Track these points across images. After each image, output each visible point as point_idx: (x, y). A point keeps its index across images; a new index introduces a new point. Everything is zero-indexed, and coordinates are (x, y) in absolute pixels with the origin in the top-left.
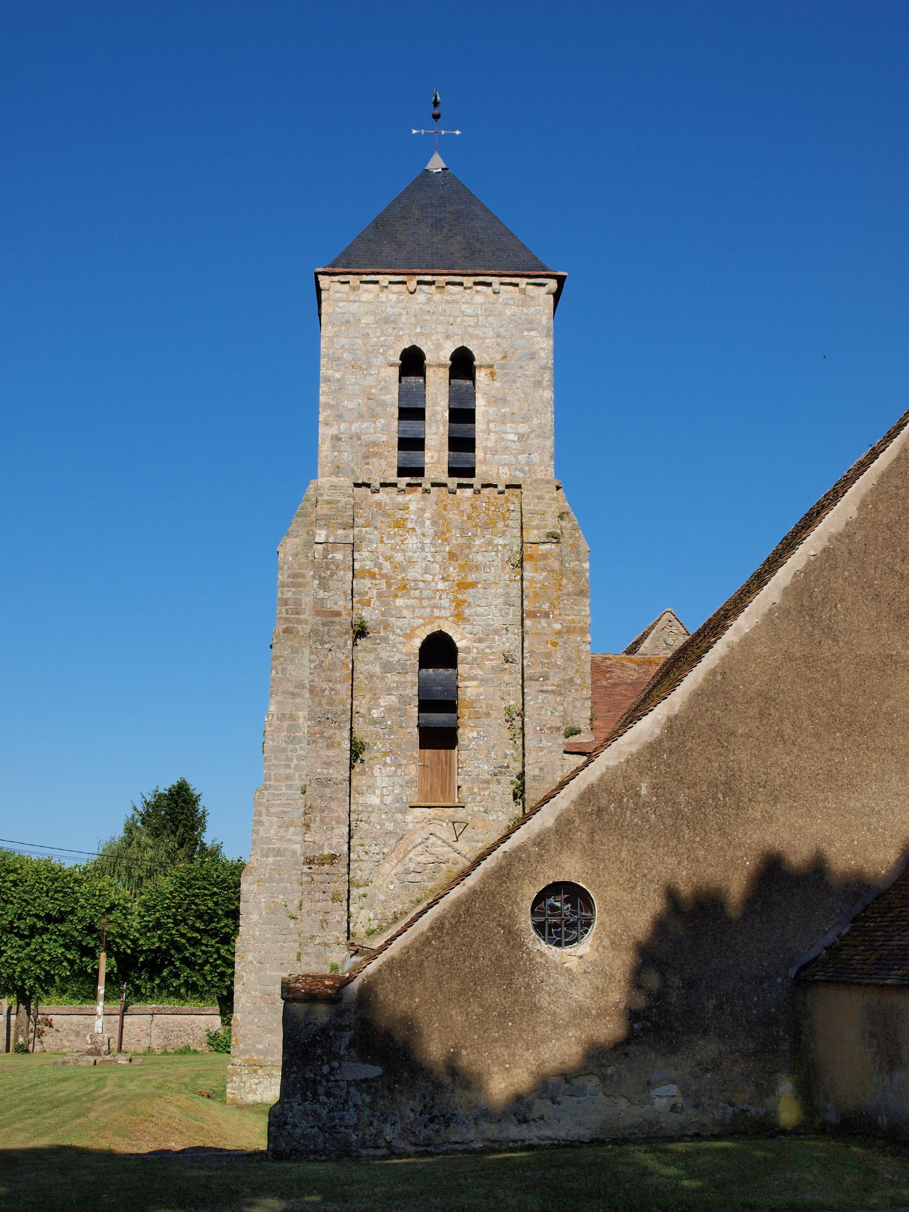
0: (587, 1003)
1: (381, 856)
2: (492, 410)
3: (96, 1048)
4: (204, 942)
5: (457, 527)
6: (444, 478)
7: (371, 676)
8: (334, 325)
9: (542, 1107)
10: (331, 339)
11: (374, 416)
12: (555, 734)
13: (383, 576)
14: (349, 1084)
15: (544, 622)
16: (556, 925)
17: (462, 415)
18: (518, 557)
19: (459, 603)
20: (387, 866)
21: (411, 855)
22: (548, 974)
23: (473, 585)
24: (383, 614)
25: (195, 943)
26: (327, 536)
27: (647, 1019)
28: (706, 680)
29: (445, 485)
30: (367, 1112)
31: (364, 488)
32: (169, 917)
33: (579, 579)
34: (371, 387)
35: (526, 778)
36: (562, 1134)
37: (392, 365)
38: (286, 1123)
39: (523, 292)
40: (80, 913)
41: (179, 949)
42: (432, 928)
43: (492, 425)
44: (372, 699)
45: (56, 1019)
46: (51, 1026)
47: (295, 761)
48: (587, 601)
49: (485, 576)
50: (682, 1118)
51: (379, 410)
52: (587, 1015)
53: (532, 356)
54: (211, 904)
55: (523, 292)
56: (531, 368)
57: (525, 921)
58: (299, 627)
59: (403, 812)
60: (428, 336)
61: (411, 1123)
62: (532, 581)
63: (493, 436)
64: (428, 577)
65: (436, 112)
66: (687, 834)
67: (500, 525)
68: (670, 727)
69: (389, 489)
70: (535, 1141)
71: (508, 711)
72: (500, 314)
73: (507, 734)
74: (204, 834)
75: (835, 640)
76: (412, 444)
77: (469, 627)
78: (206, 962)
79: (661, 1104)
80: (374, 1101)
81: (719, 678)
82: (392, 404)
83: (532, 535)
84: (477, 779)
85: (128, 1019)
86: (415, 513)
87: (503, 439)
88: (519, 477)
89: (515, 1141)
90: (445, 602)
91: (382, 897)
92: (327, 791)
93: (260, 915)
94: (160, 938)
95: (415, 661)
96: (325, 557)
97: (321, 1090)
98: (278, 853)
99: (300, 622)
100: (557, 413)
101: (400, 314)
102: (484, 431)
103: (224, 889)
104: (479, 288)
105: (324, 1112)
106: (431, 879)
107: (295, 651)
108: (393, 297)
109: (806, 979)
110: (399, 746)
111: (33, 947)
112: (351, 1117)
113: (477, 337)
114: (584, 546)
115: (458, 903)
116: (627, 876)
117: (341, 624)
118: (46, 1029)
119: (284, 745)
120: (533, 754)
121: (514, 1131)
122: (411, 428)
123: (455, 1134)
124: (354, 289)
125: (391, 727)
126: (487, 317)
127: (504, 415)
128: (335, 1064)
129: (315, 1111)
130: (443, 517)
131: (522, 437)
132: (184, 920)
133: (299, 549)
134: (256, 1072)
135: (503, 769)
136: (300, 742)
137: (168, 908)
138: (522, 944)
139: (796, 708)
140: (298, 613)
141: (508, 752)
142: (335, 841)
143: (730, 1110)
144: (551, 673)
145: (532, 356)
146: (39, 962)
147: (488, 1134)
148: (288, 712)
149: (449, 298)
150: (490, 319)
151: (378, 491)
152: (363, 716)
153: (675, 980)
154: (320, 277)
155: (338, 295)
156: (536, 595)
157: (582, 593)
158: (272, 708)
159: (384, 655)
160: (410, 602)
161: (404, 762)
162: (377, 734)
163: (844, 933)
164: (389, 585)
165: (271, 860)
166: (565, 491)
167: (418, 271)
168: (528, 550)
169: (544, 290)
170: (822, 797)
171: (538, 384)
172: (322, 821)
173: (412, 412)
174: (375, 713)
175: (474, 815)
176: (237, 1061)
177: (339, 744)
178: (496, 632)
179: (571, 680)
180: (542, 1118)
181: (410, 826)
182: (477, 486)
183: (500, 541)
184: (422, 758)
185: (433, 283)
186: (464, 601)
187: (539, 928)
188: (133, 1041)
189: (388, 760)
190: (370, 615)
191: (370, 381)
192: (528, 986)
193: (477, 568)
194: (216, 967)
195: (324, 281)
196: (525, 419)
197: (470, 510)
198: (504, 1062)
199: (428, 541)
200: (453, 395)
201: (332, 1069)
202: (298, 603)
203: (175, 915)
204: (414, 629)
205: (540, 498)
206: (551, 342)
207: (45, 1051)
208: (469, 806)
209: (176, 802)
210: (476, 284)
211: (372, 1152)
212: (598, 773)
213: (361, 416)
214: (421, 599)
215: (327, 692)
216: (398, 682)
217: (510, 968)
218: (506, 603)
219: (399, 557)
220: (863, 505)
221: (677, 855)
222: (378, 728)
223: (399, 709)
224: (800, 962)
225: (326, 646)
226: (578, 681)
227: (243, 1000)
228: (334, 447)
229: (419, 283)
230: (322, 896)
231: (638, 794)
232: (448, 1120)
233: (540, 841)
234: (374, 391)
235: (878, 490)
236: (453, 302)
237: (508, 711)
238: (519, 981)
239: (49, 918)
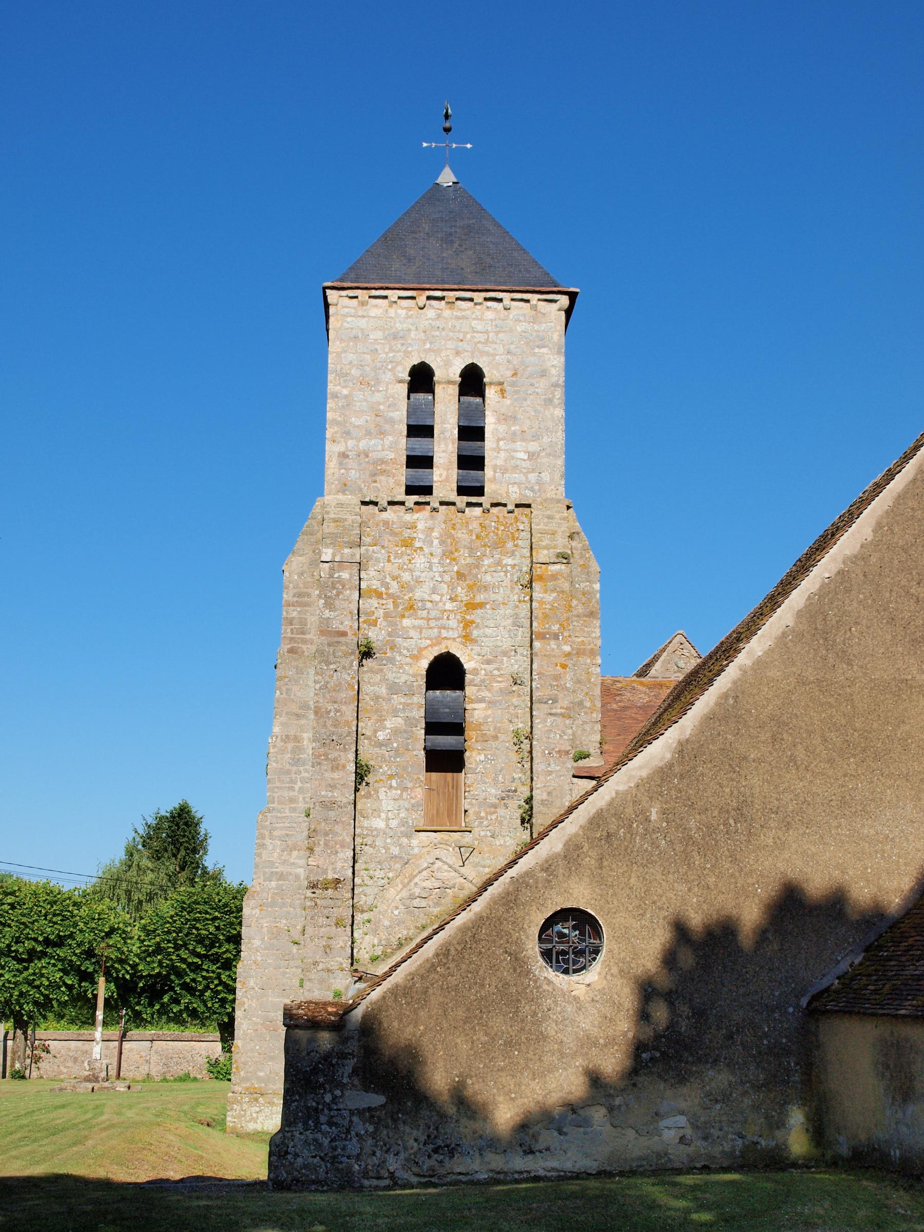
0: (595, 1032)
1: (386, 880)
2: (502, 428)
3: (94, 1075)
4: (205, 967)
5: (465, 547)
6: (453, 496)
7: (377, 698)
8: (342, 340)
9: (548, 1138)
10: (339, 355)
11: (382, 433)
12: (564, 758)
13: (390, 596)
14: (352, 1113)
15: (553, 644)
16: (564, 953)
17: (471, 433)
18: (527, 577)
19: (467, 624)
21: (416, 880)
22: (555, 1002)
23: (481, 605)
24: (389, 635)
25: (196, 968)
26: (334, 555)
27: (656, 1048)
28: (718, 704)
29: (454, 504)
30: (370, 1142)
31: (371, 507)
32: (169, 941)
33: (590, 600)
34: (379, 403)
35: (534, 803)
36: (568, 1166)
37: (401, 382)
38: (287, 1153)
39: (534, 308)
40: (79, 938)
41: (180, 974)
42: (437, 955)
43: (501, 443)
45: (53, 1045)
46: (48, 1052)
47: (299, 784)
48: (597, 623)
49: (493, 597)
50: (690, 1150)
51: (387, 427)
52: (595, 1044)
53: (543, 374)
54: (212, 929)
55: (534, 308)
56: (542, 385)
57: (532, 948)
58: (304, 647)
59: (408, 836)
60: (437, 352)
61: (415, 1154)
62: (541, 602)
63: (503, 454)
64: (436, 598)
65: (448, 125)
66: (697, 860)
67: (510, 545)
68: (681, 751)
69: (396, 507)
70: (542, 1173)
71: (516, 734)
72: (511, 331)
73: (515, 757)
74: (205, 857)
75: (850, 663)
76: (420, 462)
77: (477, 649)
78: (207, 987)
79: (670, 1136)
80: (375, 1132)
81: (731, 701)
82: (401, 421)
83: (542, 555)
84: (484, 803)
85: (126, 1045)
86: (423, 532)
87: (513, 458)
89: (521, 1173)
90: (453, 623)
92: (332, 814)
93: (263, 939)
94: (160, 963)
95: (422, 682)
97: (323, 1119)
98: (281, 877)
99: (305, 642)
100: (568, 431)
101: (409, 330)
102: (494, 449)
103: (225, 913)
104: (490, 304)
105: (326, 1142)
106: (437, 904)
107: (300, 671)
108: (403, 313)
109: (819, 1008)
110: (405, 769)
111: (31, 971)
112: (353, 1147)
113: (488, 354)
114: (595, 567)
115: (464, 930)
116: (637, 902)
117: (347, 644)
118: (43, 1054)
119: (288, 767)
120: (542, 778)
121: (520, 1163)
122: (420, 446)
123: (459, 1165)
124: (363, 304)
125: (397, 750)
126: (497, 333)
127: (514, 433)
128: (338, 1093)
129: (316, 1140)
130: (452, 537)
131: (532, 456)
132: (185, 945)
133: (305, 568)
134: (256, 1100)
135: (510, 793)
136: (304, 764)
137: (169, 932)
138: (529, 972)
139: (810, 733)
140: (303, 633)
141: (516, 776)
143: (739, 1142)
144: (561, 695)
145: (543, 374)
146: (38, 987)
147: (493, 1166)
148: (292, 733)
149: (459, 314)
150: (501, 336)
151: (385, 510)
152: (369, 738)
153: (685, 1010)
154: (328, 292)
155: (346, 310)
156: (546, 616)
157: (592, 614)
158: (276, 730)
159: (390, 676)
160: (417, 622)
161: (410, 785)
162: (383, 756)
163: (857, 962)
164: (396, 605)
165: (273, 884)
166: (576, 511)
167: (428, 286)
168: (538, 570)
169: (555, 306)
170: (835, 823)
171: (549, 402)
172: (326, 845)
173: (420, 430)
174: (381, 736)
176: (237, 1088)
177: (344, 767)
178: (505, 654)
179: (581, 703)
180: (548, 1149)
181: (416, 850)
182: (486, 505)
183: (510, 561)
184: (429, 781)
185: (443, 298)
186: (472, 622)
187: (547, 955)
188: (132, 1068)
189: (394, 783)
190: (376, 635)
191: (378, 397)
192: (535, 1014)
193: (486, 588)
195: (332, 295)
196: (536, 437)
197: (478, 530)
198: (510, 1091)
199: (435, 560)
200: (463, 412)
201: (335, 1098)
202: (303, 622)
203: (175, 939)
204: (421, 650)
205: (550, 517)
206: (563, 359)
207: (42, 1077)
208: (476, 831)
209: (177, 825)
210: (486, 299)
211: (375, 1182)
212: (608, 798)
213: (369, 433)
215: (332, 714)
216: (404, 704)
217: (516, 996)
218: (515, 624)
219: (406, 577)
220: (879, 526)
221: (687, 881)
222: (383, 751)
223: (405, 731)
224: (813, 991)
225: (332, 667)
226: (588, 704)
227: (244, 1027)
228: (341, 464)
229: (429, 298)
231: (647, 820)
232: (452, 1151)
233: (548, 866)
234: (382, 407)
235: (893, 512)
236: (464, 318)
237: (516, 734)
238: (526, 1009)
239: (47, 942)
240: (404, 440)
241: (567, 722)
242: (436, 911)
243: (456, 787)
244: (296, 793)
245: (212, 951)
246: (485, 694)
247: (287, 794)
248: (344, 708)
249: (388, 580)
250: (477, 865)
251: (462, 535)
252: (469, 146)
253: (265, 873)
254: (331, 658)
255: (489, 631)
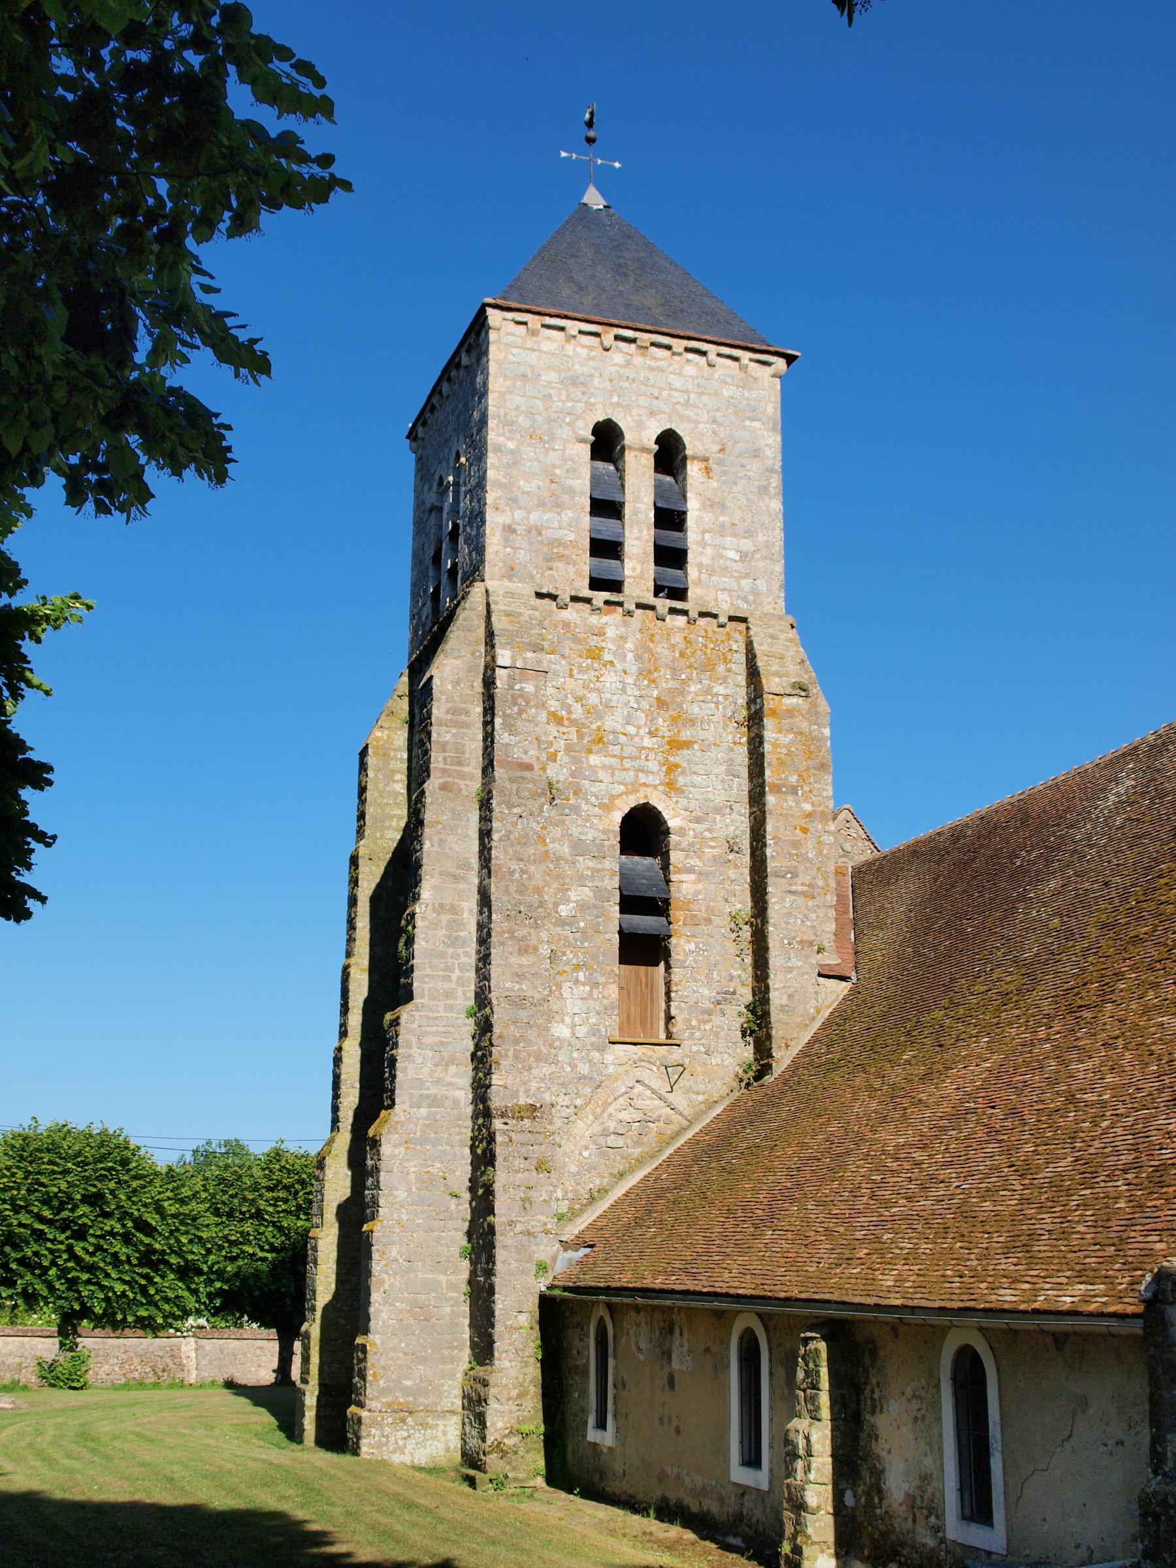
1: (572, 1110)
2: (708, 517)
4: (51, 1236)
8: (506, 377)
10: (502, 395)
11: (559, 506)
12: (808, 951)
13: (573, 722)
17: (670, 518)
19: (672, 768)
20: (580, 1124)
21: (611, 1109)
23: (688, 744)
24: (573, 774)
25: (40, 1236)
26: (514, 659)
31: (547, 601)
34: (554, 466)
37: (582, 441)
43: (707, 536)
44: (559, 890)
48: (829, 778)
49: (702, 734)
51: (565, 498)
54: (64, 1186)
55: (743, 368)
56: (754, 468)
58: (462, 783)
60: (627, 408)
62: (775, 745)
63: (709, 551)
64: (631, 730)
65: (592, 134)
67: (721, 668)
69: (580, 605)
72: (717, 394)
73: (732, 949)
76: (606, 548)
77: (683, 801)
82: (582, 493)
84: (695, 1007)
86: (614, 641)
87: (722, 557)
88: (743, 610)
90: (653, 765)
91: (574, 1168)
92: (523, 1014)
93: (409, 1190)
95: (615, 840)
96: (511, 688)
98: (434, 1102)
99: (462, 776)
102: (698, 543)
104: (690, 356)
106: (637, 1143)
107: (457, 816)
108: (583, 352)
110: (594, 957)
113: (688, 420)
117: (534, 781)
119: (442, 948)
120: (780, 976)
122: (607, 528)
124: (533, 333)
126: (700, 394)
127: (723, 525)
130: (648, 650)
131: (745, 556)
134: (403, 1421)
136: (463, 945)
140: (460, 764)
141: (734, 973)
142: (534, 1085)
144: (801, 868)
145: (756, 454)
148: (447, 900)
149: (653, 363)
150: (704, 398)
151: (564, 607)
154: (489, 311)
155: (511, 338)
156: (781, 763)
157: (822, 767)
159: (574, 830)
161: (602, 980)
162: (566, 939)
164: (580, 736)
165: (424, 1111)
167: (616, 322)
168: (769, 702)
171: (764, 490)
172: (516, 1057)
173: (606, 507)
174: (564, 911)
175: (693, 1056)
177: (536, 949)
178: (718, 810)
181: (611, 1069)
182: (693, 614)
183: (721, 690)
185: (633, 341)
186: (677, 766)
189: (581, 976)
190: (558, 772)
191: (553, 458)
193: (692, 722)
194: (69, 1270)
195: (494, 317)
196: (749, 534)
197: (682, 645)
199: (630, 680)
202: (460, 749)
204: (613, 798)
205: (773, 637)
206: (779, 438)
208: (685, 1044)
210: (687, 350)
213: (541, 504)
214: (622, 758)
215: (517, 875)
218: (729, 772)
219: (593, 699)
222: (566, 932)
223: (595, 906)
225: (515, 810)
227: (384, 1316)
228: (506, 540)
229: (617, 338)
230: (523, 1164)
234: (558, 471)
240: (587, 518)
241: (810, 903)
242: (637, 1152)
243: (650, 985)
244: (453, 986)
245: (65, 1214)
246: (695, 862)
247: (441, 986)
248: (532, 868)
249: (570, 701)
250: (689, 1090)
251: (661, 649)
252: (617, 165)
253: (411, 1096)
254: (514, 799)
255: (697, 779)
